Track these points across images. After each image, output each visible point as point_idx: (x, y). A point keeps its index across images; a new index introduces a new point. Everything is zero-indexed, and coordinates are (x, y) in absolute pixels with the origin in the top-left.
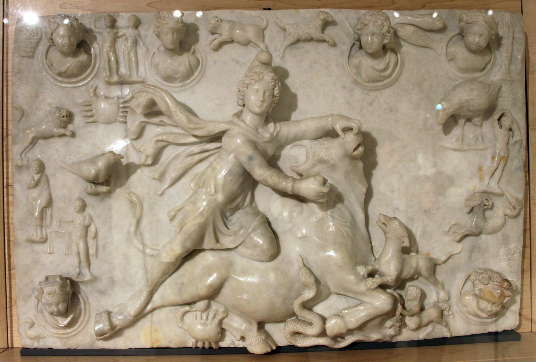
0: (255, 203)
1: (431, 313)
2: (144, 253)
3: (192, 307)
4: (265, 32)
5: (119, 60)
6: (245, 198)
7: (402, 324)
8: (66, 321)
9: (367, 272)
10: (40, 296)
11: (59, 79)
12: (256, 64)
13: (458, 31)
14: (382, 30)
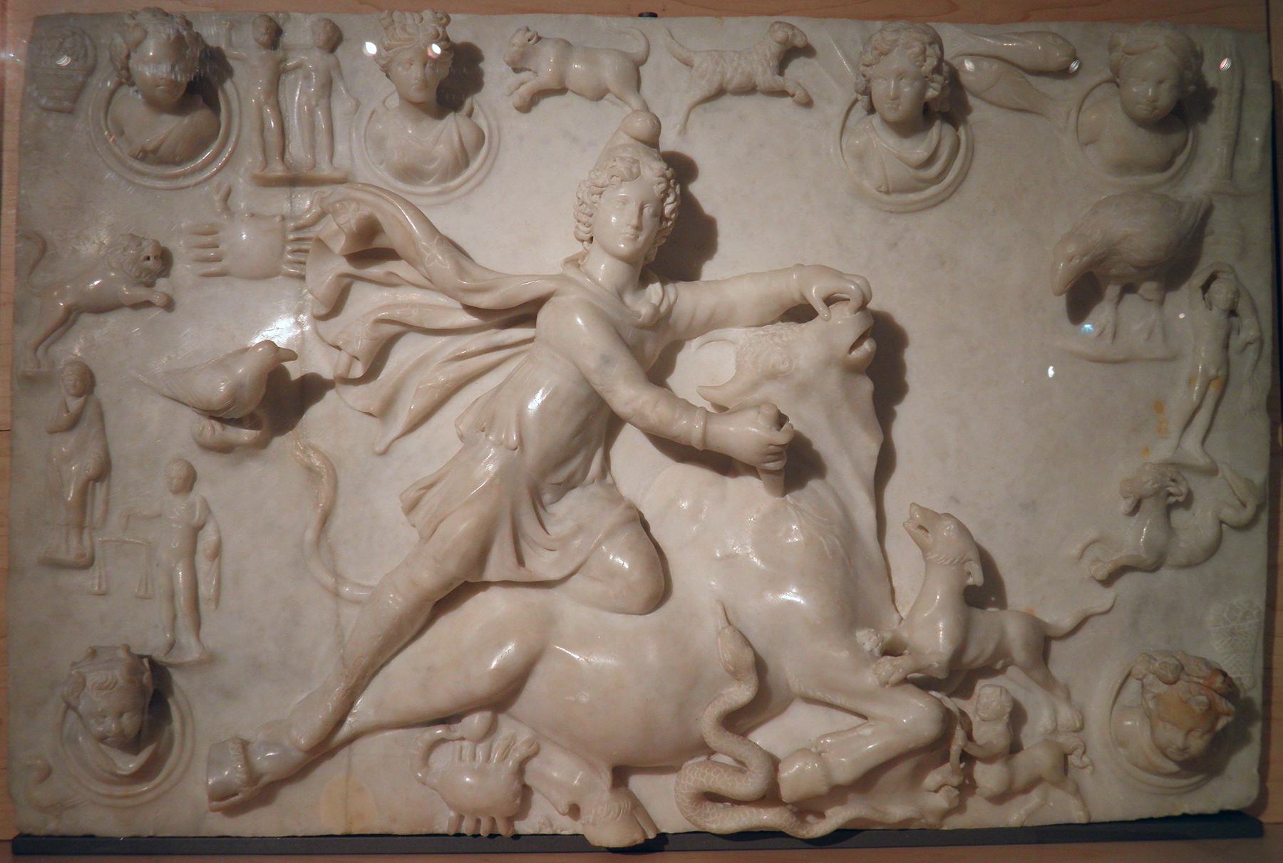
0: (611, 476)
1: (1035, 756)
2: (336, 595)
3: (451, 730)
4: (644, 70)
5: (286, 125)
6: (589, 461)
7: (967, 787)
8: (130, 764)
9: (880, 644)
10: (76, 694)
11: (138, 165)
12: (622, 142)
13: (1107, 74)
14: (923, 66)
